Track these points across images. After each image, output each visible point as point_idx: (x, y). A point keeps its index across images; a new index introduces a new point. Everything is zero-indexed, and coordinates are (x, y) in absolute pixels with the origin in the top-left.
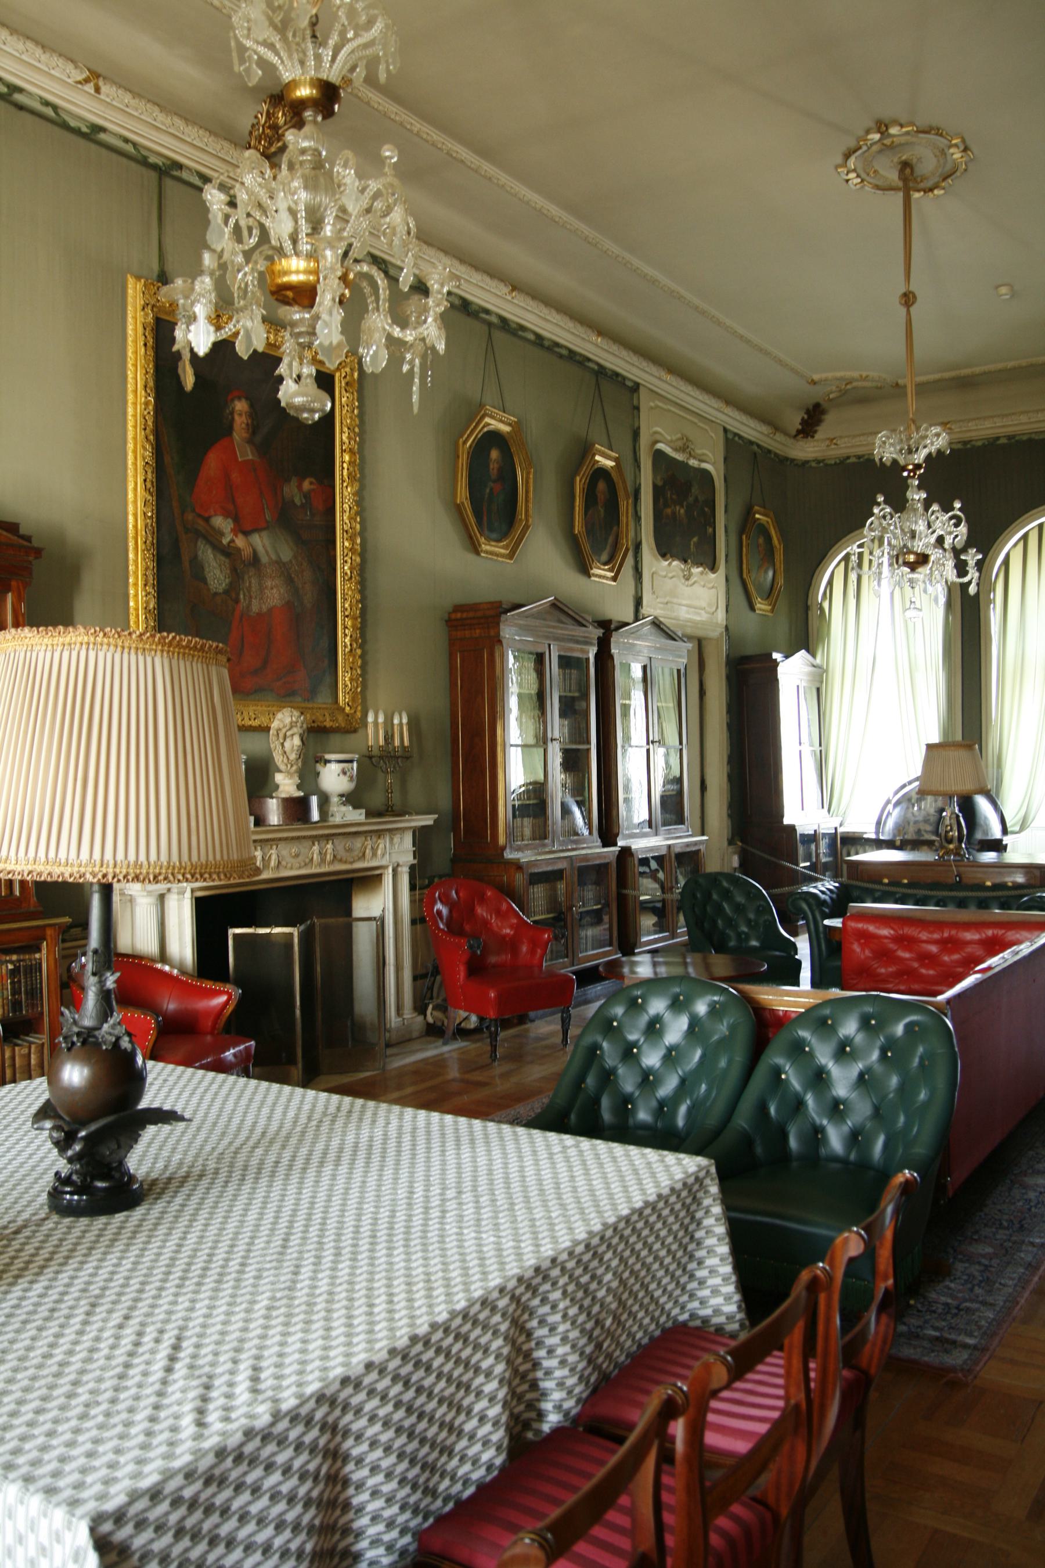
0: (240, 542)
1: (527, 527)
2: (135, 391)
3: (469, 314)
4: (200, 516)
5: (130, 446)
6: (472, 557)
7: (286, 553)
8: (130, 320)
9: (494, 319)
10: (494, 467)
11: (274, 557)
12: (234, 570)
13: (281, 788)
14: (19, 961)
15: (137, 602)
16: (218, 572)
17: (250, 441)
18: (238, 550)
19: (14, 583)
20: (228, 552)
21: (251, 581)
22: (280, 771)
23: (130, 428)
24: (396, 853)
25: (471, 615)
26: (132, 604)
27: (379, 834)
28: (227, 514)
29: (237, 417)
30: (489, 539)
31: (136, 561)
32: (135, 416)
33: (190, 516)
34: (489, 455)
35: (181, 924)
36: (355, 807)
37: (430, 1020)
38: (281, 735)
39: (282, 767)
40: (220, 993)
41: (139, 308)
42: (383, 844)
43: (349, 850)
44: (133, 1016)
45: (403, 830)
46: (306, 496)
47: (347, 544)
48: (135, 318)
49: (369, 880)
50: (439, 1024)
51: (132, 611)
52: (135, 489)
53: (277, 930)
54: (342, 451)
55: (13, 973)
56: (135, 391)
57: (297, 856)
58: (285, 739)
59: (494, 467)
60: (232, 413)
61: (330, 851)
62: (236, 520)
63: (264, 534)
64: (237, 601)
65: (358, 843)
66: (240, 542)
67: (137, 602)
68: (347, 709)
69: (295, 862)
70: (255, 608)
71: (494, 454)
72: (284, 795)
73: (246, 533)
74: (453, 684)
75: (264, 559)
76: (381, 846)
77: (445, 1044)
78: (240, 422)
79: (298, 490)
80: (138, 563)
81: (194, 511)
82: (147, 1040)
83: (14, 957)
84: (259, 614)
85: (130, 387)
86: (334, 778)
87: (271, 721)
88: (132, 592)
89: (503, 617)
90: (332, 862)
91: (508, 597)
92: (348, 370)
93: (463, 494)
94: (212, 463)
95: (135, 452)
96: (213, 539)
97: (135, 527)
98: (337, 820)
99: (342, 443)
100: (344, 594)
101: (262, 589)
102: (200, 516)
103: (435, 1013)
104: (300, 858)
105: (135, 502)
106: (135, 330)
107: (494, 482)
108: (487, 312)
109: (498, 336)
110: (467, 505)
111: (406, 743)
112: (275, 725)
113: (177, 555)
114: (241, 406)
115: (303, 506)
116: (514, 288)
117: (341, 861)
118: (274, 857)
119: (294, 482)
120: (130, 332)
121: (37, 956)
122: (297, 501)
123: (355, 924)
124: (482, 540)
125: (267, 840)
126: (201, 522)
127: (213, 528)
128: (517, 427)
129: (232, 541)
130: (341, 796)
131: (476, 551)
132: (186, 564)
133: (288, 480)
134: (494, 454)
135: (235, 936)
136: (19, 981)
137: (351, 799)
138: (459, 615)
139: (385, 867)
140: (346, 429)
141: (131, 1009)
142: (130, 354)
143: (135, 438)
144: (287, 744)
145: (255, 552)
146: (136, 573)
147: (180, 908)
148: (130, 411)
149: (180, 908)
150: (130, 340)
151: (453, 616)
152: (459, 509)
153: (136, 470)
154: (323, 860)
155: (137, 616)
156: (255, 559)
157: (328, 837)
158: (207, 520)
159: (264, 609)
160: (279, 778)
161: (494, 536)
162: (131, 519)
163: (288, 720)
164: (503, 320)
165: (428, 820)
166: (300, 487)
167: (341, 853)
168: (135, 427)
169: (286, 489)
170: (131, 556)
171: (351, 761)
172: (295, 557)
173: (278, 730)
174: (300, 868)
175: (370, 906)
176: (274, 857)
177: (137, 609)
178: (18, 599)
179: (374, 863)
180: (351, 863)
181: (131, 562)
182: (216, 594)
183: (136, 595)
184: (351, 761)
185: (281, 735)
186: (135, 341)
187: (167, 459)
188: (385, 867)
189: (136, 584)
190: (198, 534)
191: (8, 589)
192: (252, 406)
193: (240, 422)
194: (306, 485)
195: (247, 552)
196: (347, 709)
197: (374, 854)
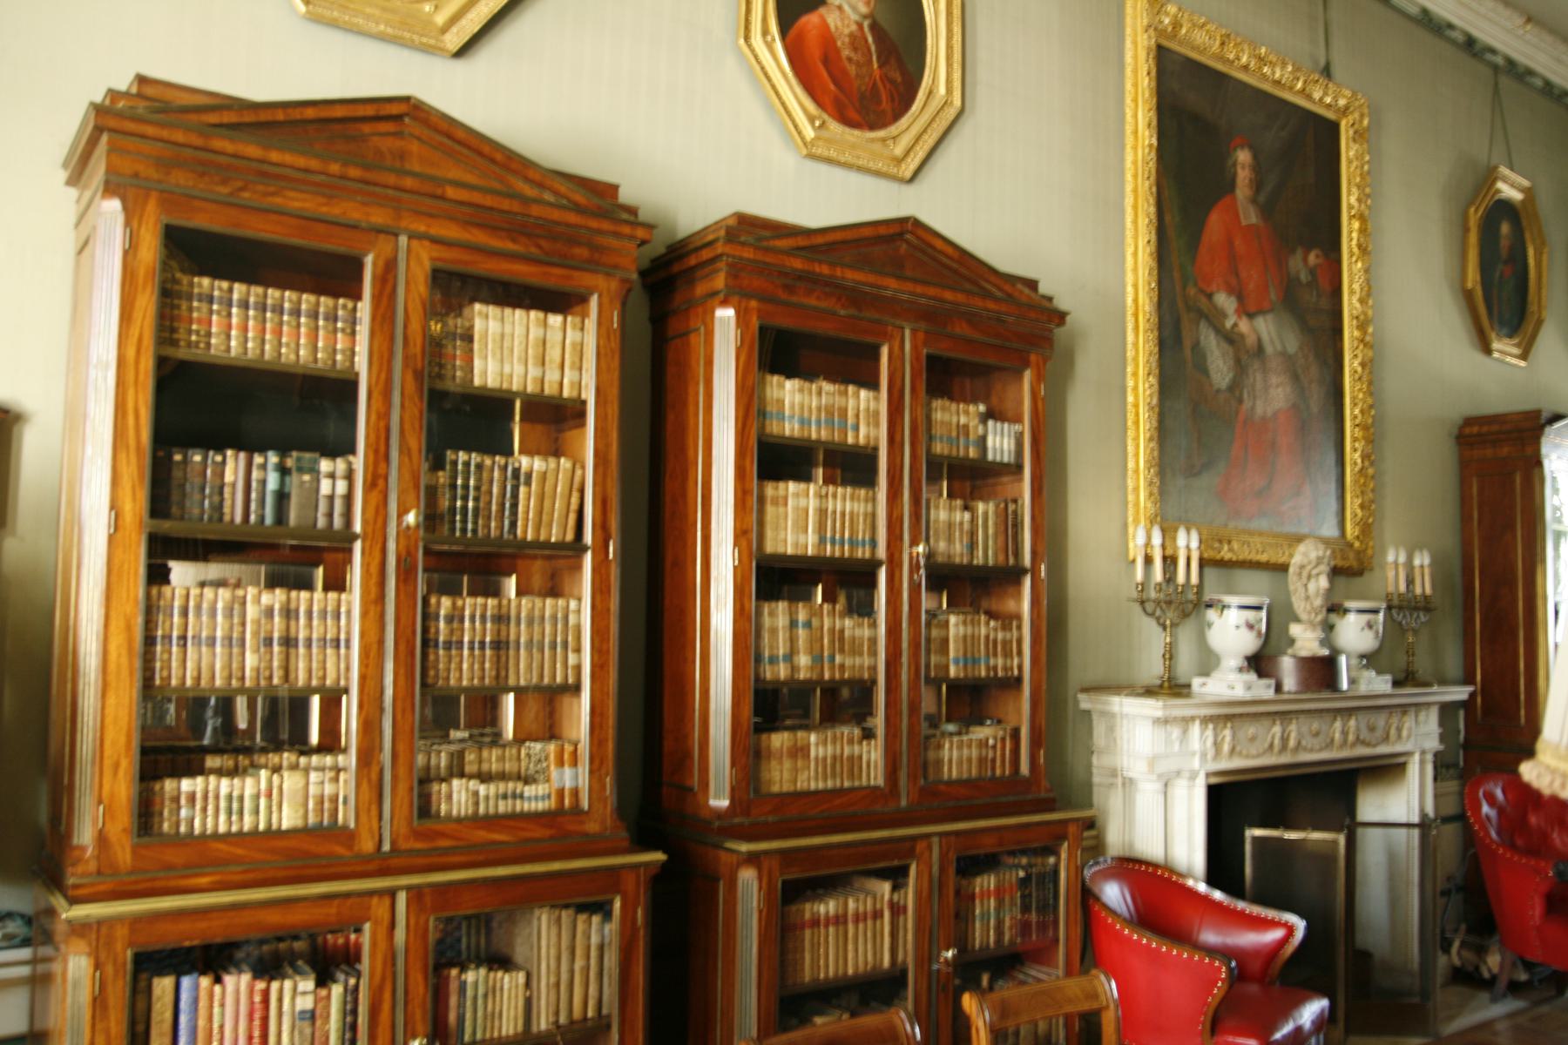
0: (1244, 326)
1: (1539, 323)
2: (1136, 132)
3: (1475, 55)
4: (1202, 291)
5: (1129, 200)
6: (1479, 357)
7: (1292, 343)
8: (1128, 44)
9: (1499, 60)
10: (1504, 243)
11: (1279, 347)
12: (1238, 361)
13: (1298, 644)
14: (1030, 865)
15: (1136, 397)
16: (1220, 363)
17: (1254, 201)
18: (1242, 336)
19: (1033, 358)
20: (1231, 339)
21: (1256, 377)
22: (1297, 620)
23: (1129, 177)
24: (1421, 738)
25: (1495, 428)
26: (1130, 399)
27: (1404, 709)
28: (1230, 291)
29: (1240, 171)
30: (1499, 337)
31: (1136, 344)
32: (1135, 163)
33: (1192, 291)
34: (1498, 229)
35: (1190, 819)
36: (1379, 672)
37: (1456, 961)
38: (1305, 574)
39: (1304, 616)
40: (1273, 924)
41: (1139, 30)
42: (1409, 722)
43: (1372, 729)
44: (1169, 951)
45: (1429, 704)
46: (1312, 272)
47: (1356, 333)
48: (1135, 43)
49: (1387, 770)
50: (1470, 969)
51: (1129, 407)
52: (1135, 254)
53: (1316, 835)
54: (1351, 217)
55: (1024, 883)
56: (1136, 132)
57: (1317, 734)
58: (1309, 577)
59: (1504, 243)
60: (1235, 165)
61: (1352, 730)
62: (1241, 298)
63: (1269, 317)
64: (1241, 401)
65: (1380, 720)
66: (1244, 326)
67: (1136, 397)
68: (1357, 544)
69: (1316, 742)
70: (1259, 410)
71: (1505, 228)
72: (1304, 653)
73: (1251, 316)
74: (1465, 518)
75: (1269, 349)
76: (1406, 725)
77: (1494, 1000)
78: (1243, 176)
79: (1304, 263)
80: (1140, 347)
81: (1196, 284)
82: (1210, 993)
83: (1024, 861)
84: (1264, 419)
85: (1129, 129)
86: (1355, 634)
87: (1291, 556)
88: (1130, 383)
89: (1548, 430)
90: (1353, 745)
91: (1548, 408)
92: (1356, 115)
93: (1473, 277)
94: (1215, 221)
95: (1135, 207)
96: (1214, 318)
97: (1136, 300)
98: (1363, 688)
99: (1350, 207)
100: (1353, 398)
101: (1266, 388)
102: (1202, 291)
103: (1465, 954)
104: (1321, 737)
105: (1135, 270)
106: (1135, 57)
107: (1506, 262)
108: (1493, 51)
109: (1505, 82)
110: (1479, 293)
111: (1428, 591)
112: (1297, 560)
113: (1178, 339)
114: (1243, 156)
115: (1309, 284)
116: (1529, 20)
117: (1305, 749)
118: (1228, 739)
119: (1299, 252)
120: (1129, 59)
121: (1052, 860)
122: (1304, 277)
123: (1360, 831)
124: (1493, 335)
125: (1290, 712)
126: (1203, 300)
127: (1215, 307)
128: (1528, 192)
129: (1235, 325)
130: (1362, 656)
131: (1488, 351)
132: (1188, 353)
133: (1293, 251)
134: (1505, 228)
135: (1255, 839)
136: (1030, 895)
137: (1370, 660)
138: (1475, 429)
139: (1409, 754)
140: (1354, 190)
141: (1149, 934)
142: (1129, 86)
143: (1135, 191)
144: (1312, 586)
145: (1259, 340)
146: (1135, 359)
147: (1190, 798)
148: (1129, 158)
149: (1190, 798)
150: (1129, 71)
151: (1467, 431)
152: (1468, 295)
153: (1136, 230)
154: (1284, 747)
155: (1137, 414)
156: (1260, 349)
157: (1350, 712)
158: (1210, 296)
159: (1269, 413)
160: (1295, 630)
161: (1505, 331)
162: (1130, 289)
163: (1313, 555)
164: (1511, 63)
165: (1460, 693)
166: (1305, 260)
167: (1364, 734)
168: (1135, 176)
169: (1292, 263)
170: (1130, 337)
171: (1376, 612)
172: (1301, 348)
173: (1302, 567)
174: (1321, 750)
175: (1376, 805)
176: (1293, 735)
177: (1136, 406)
178: (1039, 378)
179: (1398, 748)
180: (1375, 746)
181: (1129, 346)
182: (1218, 391)
183: (1135, 388)
184: (1376, 612)
185: (1305, 574)
186: (1135, 71)
187: (1168, 218)
188: (1409, 754)
189: (1135, 374)
190: (1201, 315)
191: (1026, 364)
192: (1255, 157)
193: (1243, 176)
194: (1312, 258)
195: (1251, 340)
196: (1357, 544)
197: (1399, 736)
